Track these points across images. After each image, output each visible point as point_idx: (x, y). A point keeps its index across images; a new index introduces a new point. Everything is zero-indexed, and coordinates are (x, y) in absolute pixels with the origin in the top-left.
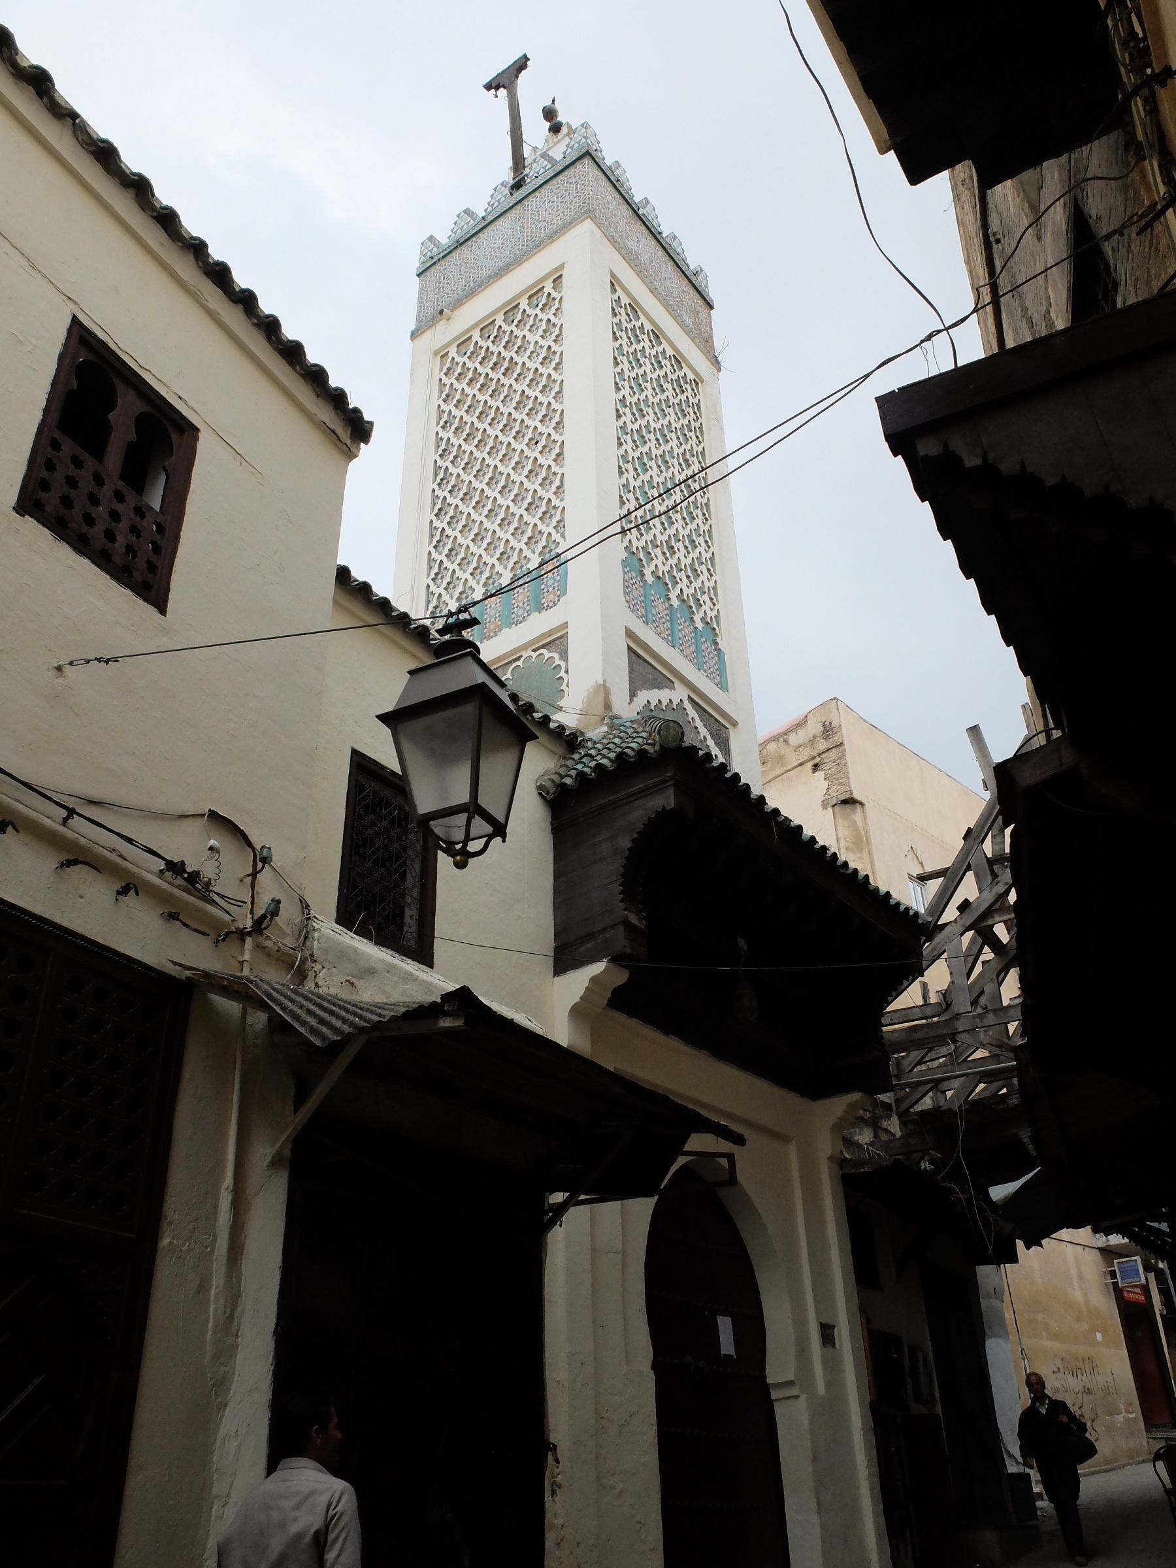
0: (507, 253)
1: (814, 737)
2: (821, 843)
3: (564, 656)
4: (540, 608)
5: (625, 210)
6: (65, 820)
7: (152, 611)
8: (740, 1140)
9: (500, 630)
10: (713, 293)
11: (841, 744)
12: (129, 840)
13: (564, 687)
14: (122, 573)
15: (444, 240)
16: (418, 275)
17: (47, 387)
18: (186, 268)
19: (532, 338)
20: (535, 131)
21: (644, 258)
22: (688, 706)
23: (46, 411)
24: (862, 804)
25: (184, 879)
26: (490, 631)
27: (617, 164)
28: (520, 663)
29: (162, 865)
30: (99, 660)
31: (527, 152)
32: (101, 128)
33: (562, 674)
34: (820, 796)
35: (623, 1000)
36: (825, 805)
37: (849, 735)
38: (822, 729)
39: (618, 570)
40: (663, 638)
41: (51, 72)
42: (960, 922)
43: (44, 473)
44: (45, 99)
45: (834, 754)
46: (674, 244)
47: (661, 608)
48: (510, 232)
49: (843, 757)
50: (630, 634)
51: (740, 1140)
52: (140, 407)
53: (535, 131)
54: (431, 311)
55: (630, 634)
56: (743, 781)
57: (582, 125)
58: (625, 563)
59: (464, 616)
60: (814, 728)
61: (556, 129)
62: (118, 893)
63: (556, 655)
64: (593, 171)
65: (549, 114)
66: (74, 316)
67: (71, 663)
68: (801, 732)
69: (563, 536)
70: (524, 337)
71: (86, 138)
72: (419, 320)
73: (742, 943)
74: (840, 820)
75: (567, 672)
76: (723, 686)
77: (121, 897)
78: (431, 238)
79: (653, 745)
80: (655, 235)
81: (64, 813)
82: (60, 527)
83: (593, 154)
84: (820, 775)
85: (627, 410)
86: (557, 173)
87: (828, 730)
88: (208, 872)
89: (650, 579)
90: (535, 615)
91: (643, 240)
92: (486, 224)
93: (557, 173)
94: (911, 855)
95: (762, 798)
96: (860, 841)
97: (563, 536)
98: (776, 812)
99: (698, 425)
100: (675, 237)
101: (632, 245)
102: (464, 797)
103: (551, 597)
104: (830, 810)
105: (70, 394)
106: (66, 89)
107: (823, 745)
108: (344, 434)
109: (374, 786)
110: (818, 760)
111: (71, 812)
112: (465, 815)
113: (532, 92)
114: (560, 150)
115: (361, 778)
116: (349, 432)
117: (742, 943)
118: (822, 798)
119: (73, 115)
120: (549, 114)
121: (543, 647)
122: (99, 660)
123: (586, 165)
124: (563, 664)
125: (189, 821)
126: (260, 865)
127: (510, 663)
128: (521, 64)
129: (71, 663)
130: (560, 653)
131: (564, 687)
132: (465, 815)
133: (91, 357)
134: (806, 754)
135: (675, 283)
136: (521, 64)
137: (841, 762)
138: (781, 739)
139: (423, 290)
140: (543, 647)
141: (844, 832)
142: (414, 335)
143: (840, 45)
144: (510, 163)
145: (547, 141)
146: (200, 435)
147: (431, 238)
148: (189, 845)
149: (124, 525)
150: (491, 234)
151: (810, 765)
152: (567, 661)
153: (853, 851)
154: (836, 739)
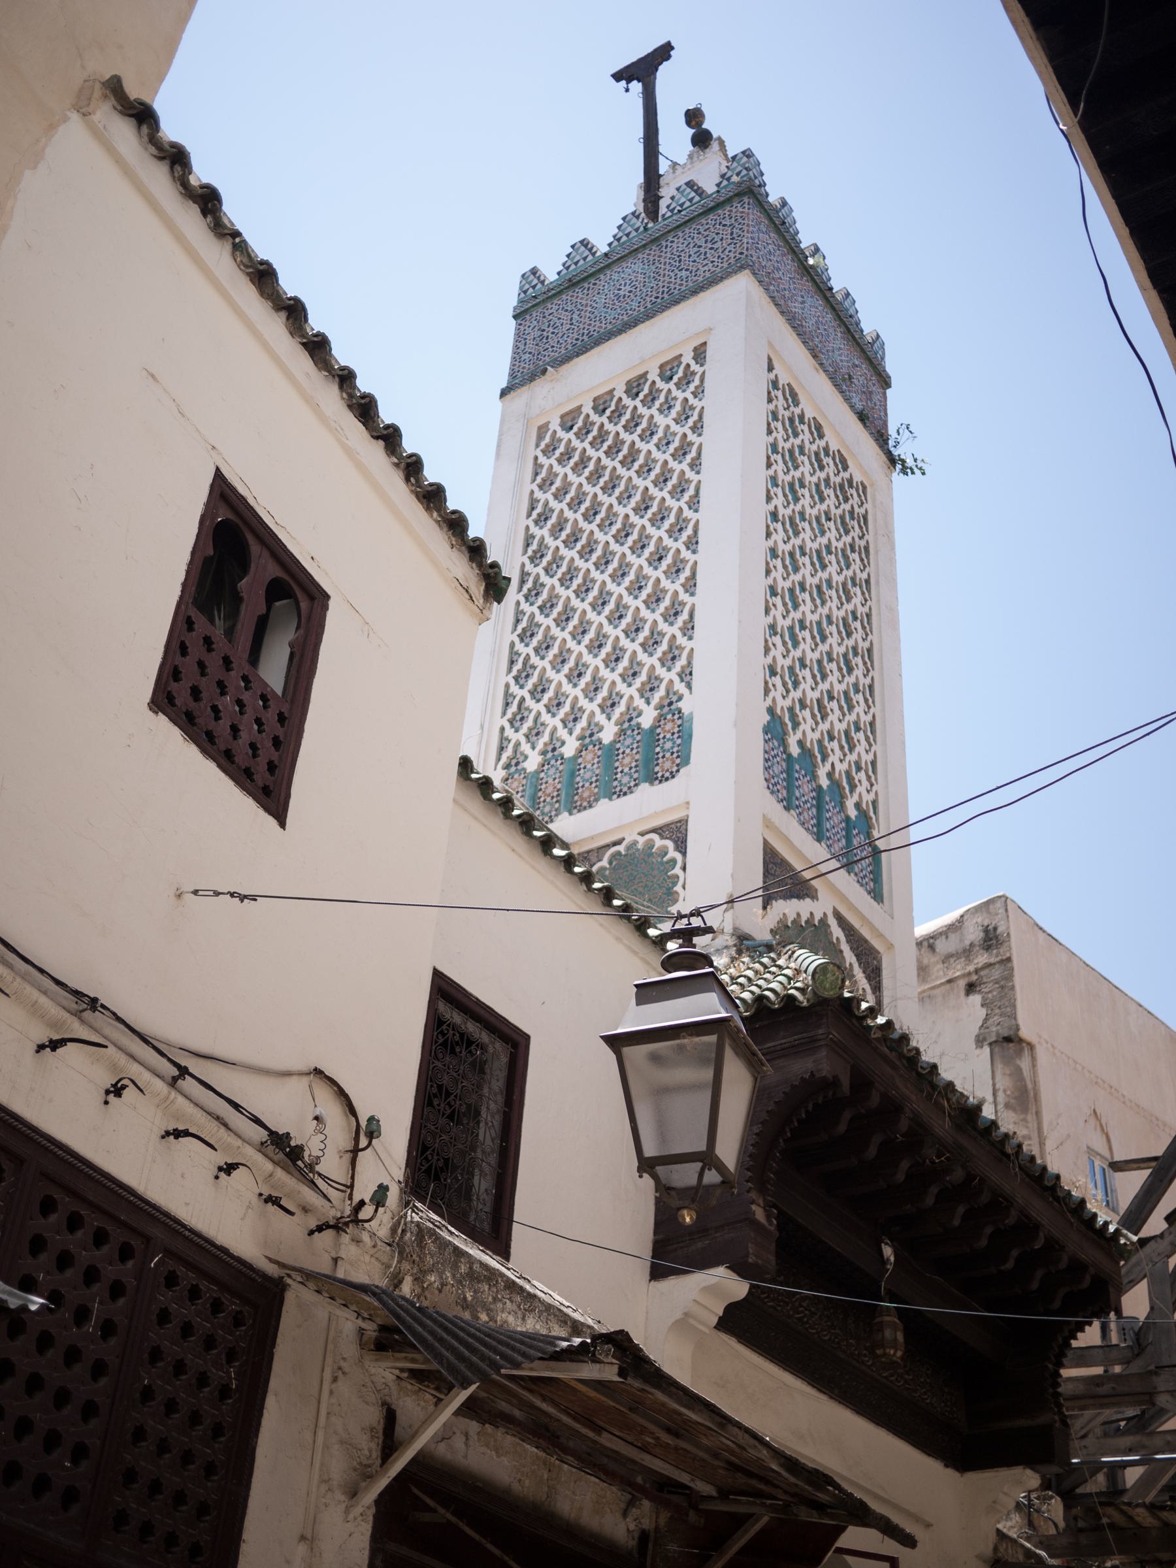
0: (635, 305)
1: (972, 945)
2: (1003, 1130)
3: (681, 846)
4: (653, 778)
5: (789, 264)
6: (175, 1079)
7: (272, 822)
8: (909, 1541)
9: (597, 800)
10: (891, 366)
11: (1009, 959)
12: (236, 1106)
13: (678, 888)
14: (243, 777)
15: (551, 275)
16: (515, 317)
17: (187, 557)
18: (331, 398)
19: (661, 421)
20: (675, 141)
21: (810, 324)
22: (832, 922)
23: (185, 585)
24: (1031, 1047)
25: (287, 1155)
26: (582, 799)
27: (784, 203)
28: (621, 848)
29: (263, 1135)
30: (232, 895)
31: (663, 166)
32: (262, 250)
33: (677, 870)
34: (974, 1029)
35: (735, 1321)
36: (979, 1041)
37: (1019, 948)
38: (982, 935)
39: (759, 737)
40: (807, 830)
41: (221, 191)
42: (1169, 1239)
43: (179, 659)
44: (209, 219)
45: (996, 973)
46: (847, 304)
47: (806, 788)
48: (640, 277)
49: (1009, 977)
50: (768, 823)
51: (909, 1541)
52: (273, 571)
53: (675, 141)
54: (528, 367)
55: (768, 823)
56: (914, 1043)
57: (743, 153)
58: (766, 730)
59: (696, 922)
60: (973, 934)
61: (702, 139)
62: (220, 1169)
63: (670, 844)
64: (753, 214)
65: (694, 117)
66: (218, 469)
67: (195, 892)
68: (953, 937)
69: (689, 686)
70: (652, 417)
71: (245, 260)
72: (513, 375)
73: (888, 1251)
74: (999, 1067)
75: (684, 869)
76: (877, 894)
77: (222, 1175)
78: (534, 271)
79: (802, 990)
80: (823, 289)
81: (176, 1072)
82: (188, 723)
83: (756, 190)
84: (976, 999)
85: (779, 526)
86: (710, 223)
87: (991, 939)
88: (313, 1148)
89: (795, 750)
90: (645, 786)
91: (809, 301)
92: (610, 261)
93: (710, 223)
94: (1092, 1121)
95: (934, 1067)
96: (1024, 1098)
97: (689, 686)
98: (950, 1085)
99: (863, 543)
100: (848, 295)
101: (795, 307)
102: (702, 1146)
103: (667, 765)
104: (987, 1050)
105: (207, 561)
106: (233, 210)
107: (982, 959)
108: (478, 589)
109: (457, 1018)
110: (974, 978)
111: (184, 1071)
112: (700, 1164)
113: (675, 89)
114: (708, 174)
115: (442, 1006)
116: (482, 588)
117: (888, 1251)
118: (976, 1031)
119: (236, 234)
120: (694, 117)
121: (654, 831)
122: (232, 895)
123: (745, 210)
124: (678, 856)
125: (294, 1079)
126: (363, 1142)
127: (608, 846)
128: (664, 52)
129: (195, 892)
130: (675, 842)
131: (678, 888)
132: (700, 1164)
133: (231, 516)
134: (958, 969)
135: (843, 355)
136: (664, 52)
137: (1006, 985)
138: (925, 944)
139: (520, 336)
140: (654, 831)
141: (1003, 1082)
142: (504, 393)
143: (1154, 294)
144: (641, 179)
145: (691, 156)
146: (331, 603)
147: (534, 271)
148: (288, 1108)
149: (249, 715)
150: (615, 277)
151: (962, 983)
152: (684, 854)
153: (1014, 1110)
154: (1003, 952)
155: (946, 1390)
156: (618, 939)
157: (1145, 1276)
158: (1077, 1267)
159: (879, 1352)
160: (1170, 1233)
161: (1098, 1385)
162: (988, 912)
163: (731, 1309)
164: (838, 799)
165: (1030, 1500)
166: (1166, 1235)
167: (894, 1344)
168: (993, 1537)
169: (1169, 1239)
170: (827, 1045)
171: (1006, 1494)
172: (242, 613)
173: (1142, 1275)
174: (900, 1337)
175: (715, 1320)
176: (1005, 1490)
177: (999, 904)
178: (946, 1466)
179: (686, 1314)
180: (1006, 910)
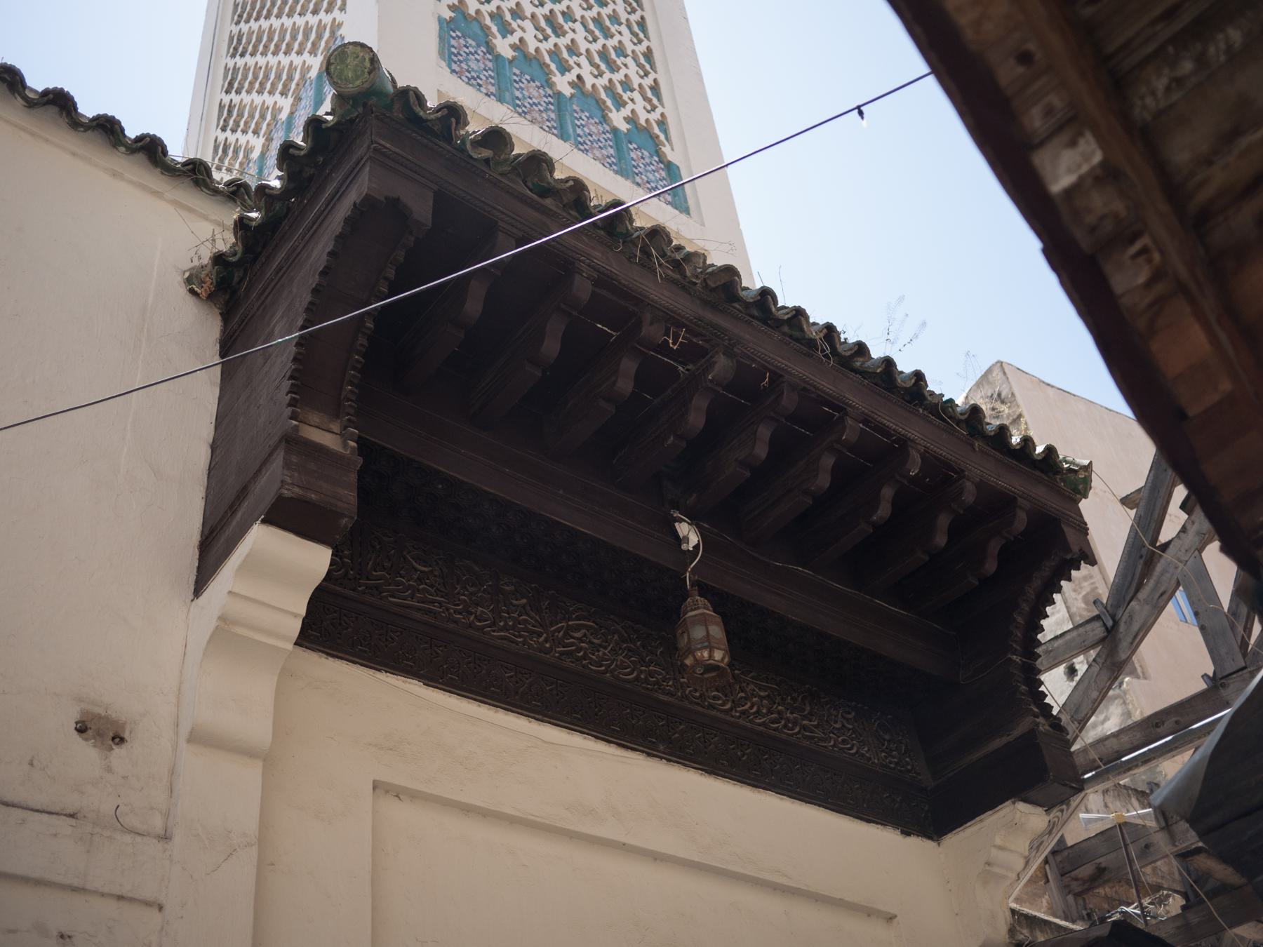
42: (1192, 530)
73: (690, 535)
155: (887, 737)
156: (115, 174)
157: (1178, 584)
158: (998, 505)
159: (688, 662)
160: (1193, 523)
161: (1157, 725)
162: (989, 383)
163: (322, 602)
164: (599, 114)
165: (1142, 908)
166: (1188, 526)
167: (709, 644)
168: (1008, 914)
169: (1192, 530)
170: (370, 157)
171: (1001, 848)
172: (1001, 813)
173: (1173, 582)
174: (717, 631)
175: (296, 626)
176: (998, 841)
177: (997, 374)
178: (906, 833)
179: (222, 618)
180: (1005, 373)
